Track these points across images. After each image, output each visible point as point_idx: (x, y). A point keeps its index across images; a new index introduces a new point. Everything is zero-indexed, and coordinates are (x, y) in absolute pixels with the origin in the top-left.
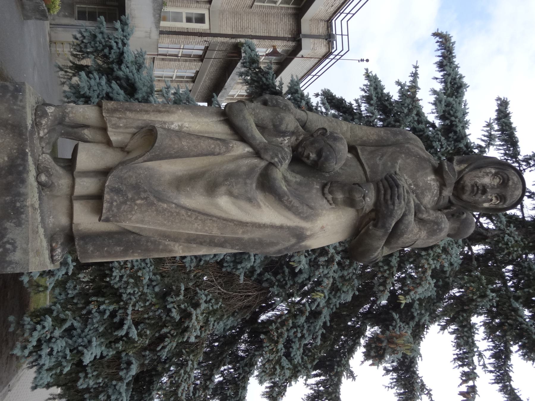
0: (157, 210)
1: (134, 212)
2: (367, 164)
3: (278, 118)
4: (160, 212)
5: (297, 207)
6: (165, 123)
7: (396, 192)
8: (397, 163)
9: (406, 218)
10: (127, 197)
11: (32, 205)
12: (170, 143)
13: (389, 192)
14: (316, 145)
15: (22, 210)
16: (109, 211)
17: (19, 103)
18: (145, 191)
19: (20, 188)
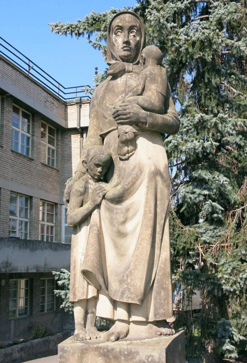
0: (134, 270)
1: (135, 284)
2: (109, 128)
3: (76, 193)
4: (135, 267)
5: (133, 178)
6: (81, 264)
7: (121, 112)
8: (108, 107)
9: (140, 102)
10: (126, 288)
11: (128, 345)
12: (90, 261)
13: (121, 117)
14: (92, 167)
15: (129, 350)
16: (133, 299)
17: (69, 349)
18: (123, 276)
19: (116, 351)
